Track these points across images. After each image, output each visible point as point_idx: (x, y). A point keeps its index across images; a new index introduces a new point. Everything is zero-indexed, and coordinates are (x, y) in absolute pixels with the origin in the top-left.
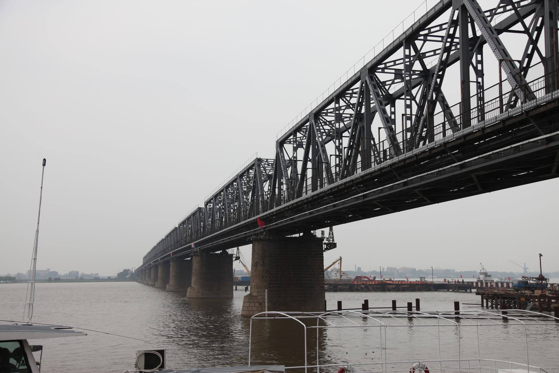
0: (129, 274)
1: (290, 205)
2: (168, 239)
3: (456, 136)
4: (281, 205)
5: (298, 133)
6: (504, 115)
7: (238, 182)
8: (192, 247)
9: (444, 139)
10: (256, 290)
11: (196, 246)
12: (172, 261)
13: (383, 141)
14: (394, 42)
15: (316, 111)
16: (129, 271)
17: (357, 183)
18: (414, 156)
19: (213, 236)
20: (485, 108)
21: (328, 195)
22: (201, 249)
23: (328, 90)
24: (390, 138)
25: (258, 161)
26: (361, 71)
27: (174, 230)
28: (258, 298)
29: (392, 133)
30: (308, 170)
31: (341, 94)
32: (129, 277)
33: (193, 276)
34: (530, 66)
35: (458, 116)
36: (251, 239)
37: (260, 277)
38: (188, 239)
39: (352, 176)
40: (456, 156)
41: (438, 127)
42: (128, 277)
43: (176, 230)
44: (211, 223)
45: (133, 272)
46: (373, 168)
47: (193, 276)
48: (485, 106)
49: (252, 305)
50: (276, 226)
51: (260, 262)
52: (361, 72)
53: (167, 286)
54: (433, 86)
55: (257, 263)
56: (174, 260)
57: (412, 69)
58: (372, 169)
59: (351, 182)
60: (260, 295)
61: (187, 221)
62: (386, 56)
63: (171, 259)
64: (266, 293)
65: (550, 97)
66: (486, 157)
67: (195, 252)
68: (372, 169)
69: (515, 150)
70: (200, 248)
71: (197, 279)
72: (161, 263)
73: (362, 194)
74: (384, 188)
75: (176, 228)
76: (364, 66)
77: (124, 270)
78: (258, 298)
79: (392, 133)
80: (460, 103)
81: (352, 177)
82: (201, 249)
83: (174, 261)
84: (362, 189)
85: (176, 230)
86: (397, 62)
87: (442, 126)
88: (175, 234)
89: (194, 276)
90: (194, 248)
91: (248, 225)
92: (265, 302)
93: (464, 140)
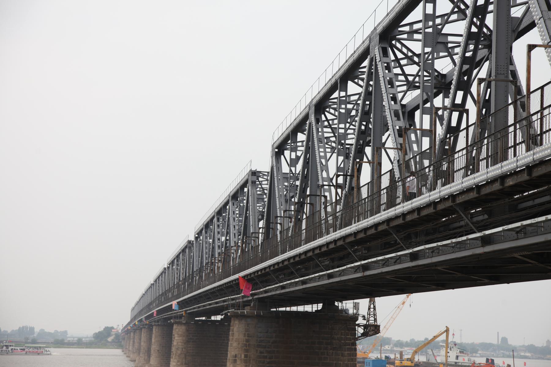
0: (112, 335)
2: (172, 269)
3: (505, 168)
4: (396, 205)
7: (310, 124)
8: (173, 308)
11: (179, 308)
12: (155, 325)
13: (542, 88)
15: (384, 28)
16: (113, 330)
18: (449, 197)
19: (270, 266)
22: (187, 312)
25: (252, 175)
27: (186, 247)
32: (113, 340)
33: (172, 358)
35: (463, 149)
36: (229, 314)
38: (218, 268)
41: (460, 154)
42: (110, 339)
43: (190, 248)
45: (120, 331)
47: (172, 358)
48: (545, 114)
50: (215, 305)
51: (241, 356)
52: (370, 39)
55: (236, 356)
61: (215, 219)
63: (155, 321)
66: (518, 230)
67: (176, 317)
70: (186, 311)
71: (179, 363)
72: (146, 324)
75: (189, 242)
77: (105, 327)
80: (368, 184)
82: (187, 312)
83: (158, 325)
85: (190, 248)
89: (174, 357)
90: (176, 310)
93: (477, 193)
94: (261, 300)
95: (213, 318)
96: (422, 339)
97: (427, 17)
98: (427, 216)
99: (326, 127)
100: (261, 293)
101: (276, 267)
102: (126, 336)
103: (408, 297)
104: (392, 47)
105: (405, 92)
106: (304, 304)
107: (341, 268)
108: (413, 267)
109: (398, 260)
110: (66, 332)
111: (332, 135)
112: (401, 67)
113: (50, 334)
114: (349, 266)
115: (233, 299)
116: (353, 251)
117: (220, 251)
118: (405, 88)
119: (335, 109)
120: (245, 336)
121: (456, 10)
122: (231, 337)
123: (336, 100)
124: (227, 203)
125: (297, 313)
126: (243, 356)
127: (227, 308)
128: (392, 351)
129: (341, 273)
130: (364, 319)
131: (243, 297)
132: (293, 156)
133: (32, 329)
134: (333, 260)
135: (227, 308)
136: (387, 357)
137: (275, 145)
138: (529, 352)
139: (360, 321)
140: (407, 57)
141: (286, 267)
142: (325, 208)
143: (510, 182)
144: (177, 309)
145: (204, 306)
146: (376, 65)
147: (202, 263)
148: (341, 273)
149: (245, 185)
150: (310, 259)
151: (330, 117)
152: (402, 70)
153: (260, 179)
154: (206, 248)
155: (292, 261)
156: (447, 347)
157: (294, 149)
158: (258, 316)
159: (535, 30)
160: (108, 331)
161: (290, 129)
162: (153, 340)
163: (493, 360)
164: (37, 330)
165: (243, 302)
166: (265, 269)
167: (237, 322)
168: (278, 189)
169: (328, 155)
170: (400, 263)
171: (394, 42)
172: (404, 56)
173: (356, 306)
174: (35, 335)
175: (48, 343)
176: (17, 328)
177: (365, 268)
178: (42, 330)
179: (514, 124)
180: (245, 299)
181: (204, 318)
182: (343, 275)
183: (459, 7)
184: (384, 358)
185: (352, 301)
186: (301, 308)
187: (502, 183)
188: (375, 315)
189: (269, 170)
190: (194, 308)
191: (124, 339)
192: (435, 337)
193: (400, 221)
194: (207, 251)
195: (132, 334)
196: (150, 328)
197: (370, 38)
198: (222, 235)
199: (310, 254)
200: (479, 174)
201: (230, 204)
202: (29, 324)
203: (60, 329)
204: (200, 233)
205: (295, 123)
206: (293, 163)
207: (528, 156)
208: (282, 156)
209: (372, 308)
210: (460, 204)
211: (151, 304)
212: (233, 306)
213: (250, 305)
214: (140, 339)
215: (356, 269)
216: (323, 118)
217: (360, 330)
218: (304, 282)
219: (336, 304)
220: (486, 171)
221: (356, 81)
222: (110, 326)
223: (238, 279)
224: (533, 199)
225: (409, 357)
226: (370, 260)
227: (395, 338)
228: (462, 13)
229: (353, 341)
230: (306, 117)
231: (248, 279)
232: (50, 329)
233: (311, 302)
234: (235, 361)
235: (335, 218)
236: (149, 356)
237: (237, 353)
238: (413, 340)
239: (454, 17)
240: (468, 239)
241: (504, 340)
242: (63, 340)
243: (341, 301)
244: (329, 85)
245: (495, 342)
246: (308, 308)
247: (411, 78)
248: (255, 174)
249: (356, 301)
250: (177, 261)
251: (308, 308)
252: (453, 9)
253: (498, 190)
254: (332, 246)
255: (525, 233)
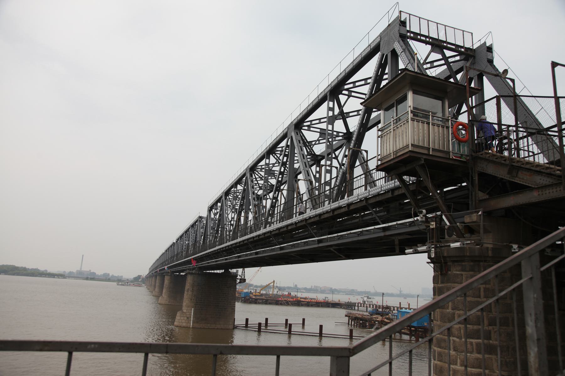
1: (256, 236)
2: (166, 253)
4: (248, 235)
5: (238, 185)
6: (377, 190)
7: (223, 200)
9: (348, 199)
10: (186, 308)
14: (277, 137)
17: (312, 222)
19: (204, 255)
20: (354, 183)
21: (275, 235)
23: (283, 124)
24: (309, 191)
26: (288, 128)
27: (172, 245)
28: (187, 314)
29: (311, 186)
30: (300, 182)
31: (271, 151)
34: (356, 166)
37: (190, 299)
38: (184, 254)
39: (288, 221)
40: (379, 215)
41: (359, 178)
42: (140, 280)
44: (288, 190)
45: (144, 277)
46: (356, 197)
48: (354, 181)
49: (182, 318)
52: (288, 128)
53: (178, 315)
54: (356, 133)
55: (188, 289)
56: (160, 275)
57: (399, 69)
58: (353, 198)
59: (252, 239)
60: (188, 312)
61: (184, 234)
62: (323, 98)
64: (192, 311)
65: (380, 189)
67: (166, 273)
68: (353, 198)
69: (263, 252)
73: (255, 251)
74: (309, 241)
75: (174, 243)
76: (291, 123)
78: (187, 314)
79: (311, 186)
81: (289, 221)
84: (238, 251)
86: (357, 84)
87: (365, 177)
88: (172, 249)
91: (219, 252)
92: (191, 317)
93: (332, 214)
94: (200, 267)
95: (181, 274)
96: (265, 285)
97: (266, 164)
98: (262, 238)
99: (229, 201)
100: (200, 265)
101: (214, 252)
102: (146, 279)
103: (260, 268)
104: (254, 173)
105: (259, 190)
106: (217, 270)
107: (230, 257)
108: (256, 257)
109: (251, 254)
110: (122, 276)
111: (231, 204)
112: (257, 181)
113: (115, 277)
114: (233, 256)
115: (189, 267)
116: (235, 251)
117: (185, 247)
118: (258, 189)
119: (232, 195)
120: (192, 281)
121: (277, 162)
122: (187, 282)
123: (233, 191)
124: (189, 228)
125: (214, 273)
126: (191, 289)
127: (186, 270)
128: (253, 289)
129: (230, 259)
130: (240, 276)
131: (193, 266)
132: (216, 211)
133: (109, 274)
134: (227, 253)
135: (186, 270)
136: (250, 292)
137: (209, 207)
138: (305, 290)
139: (239, 277)
140: (260, 177)
141: (210, 255)
142: (226, 233)
143: (290, 228)
144: (167, 269)
145: (178, 269)
146: (248, 180)
147: (178, 252)
148: (230, 259)
149: (196, 222)
150: (219, 252)
151: (230, 197)
152: (257, 182)
153: (203, 220)
154: (180, 246)
155: (212, 253)
156: (273, 288)
157: (216, 209)
158: (198, 274)
159: (301, 174)
160: (139, 277)
161: (215, 201)
162: (157, 282)
163: (290, 293)
164: (111, 275)
165: (193, 268)
166: (202, 255)
167: (190, 276)
168: (209, 224)
169: (229, 212)
170: (251, 256)
171: (255, 172)
172: (259, 177)
173: (237, 271)
174: (110, 277)
175: (115, 280)
176: (103, 274)
177: (239, 257)
178: (113, 275)
179: (296, 205)
180: (194, 267)
181: (178, 274)
182: (231, 259)
183: (278, 161)
184: (249, 292)
185: (235, 269)
186: (216, 271)
187: (287, 228)
188: (244, 275)
189: (206, 216)
190: (174, 269)
191: (145, 280)
192: (269, 284)
193: (252, 240)
194: (180, 247)
195: (149, 278)
196: (156, 277)
197: (246, 169)
198: (187, 241)
199: (219, 250)
200: (344, 200)
201: (191, 229)
202: (108, 272)
203: (120, 275)
204: (178, 240)
205: (217, 199)
206: (215, 214)
207: (328, 207)
208: (212, 212)
209: (244, 272)
210: (250, 242)
211: (158, 266)
212: (188, 269)
213: (195, 269)
214: (152, 281)
215: (236, 257)
216: (228, 198)
217: (238, 281)
218: (216, 261)
219: (229, 270)
220: (322, 208)
221: (241, 185)
222: (140, 275)
223: (191, 259)
224: (299, 234)
225: (259, 291)
226: (241, 254)
227: (255, 284)
228: (279, 163)
229: (235, 285)
230: (221, 197)
231: (195, 259)
232: (116, 275)
233: (220, 269)
234: (188, 291)
235: (230, 237)
236: (155, 287)
237: (189, 288)
238: (262, 285)
239: (277, 165)
240: (275, 248)
241: (296, 285)
242: (121, 280)
243: (231, 269)
244: (230, 186)
245: (292, 286)
246: (218, 271)
247: (261, 185)
248: (201, 217)
249: (237, 269)
250: (169, 250)
251: (218, 271)
252: (276, 162)
253: (286, 230)
254: (227, 248)
255: (294, 247)
